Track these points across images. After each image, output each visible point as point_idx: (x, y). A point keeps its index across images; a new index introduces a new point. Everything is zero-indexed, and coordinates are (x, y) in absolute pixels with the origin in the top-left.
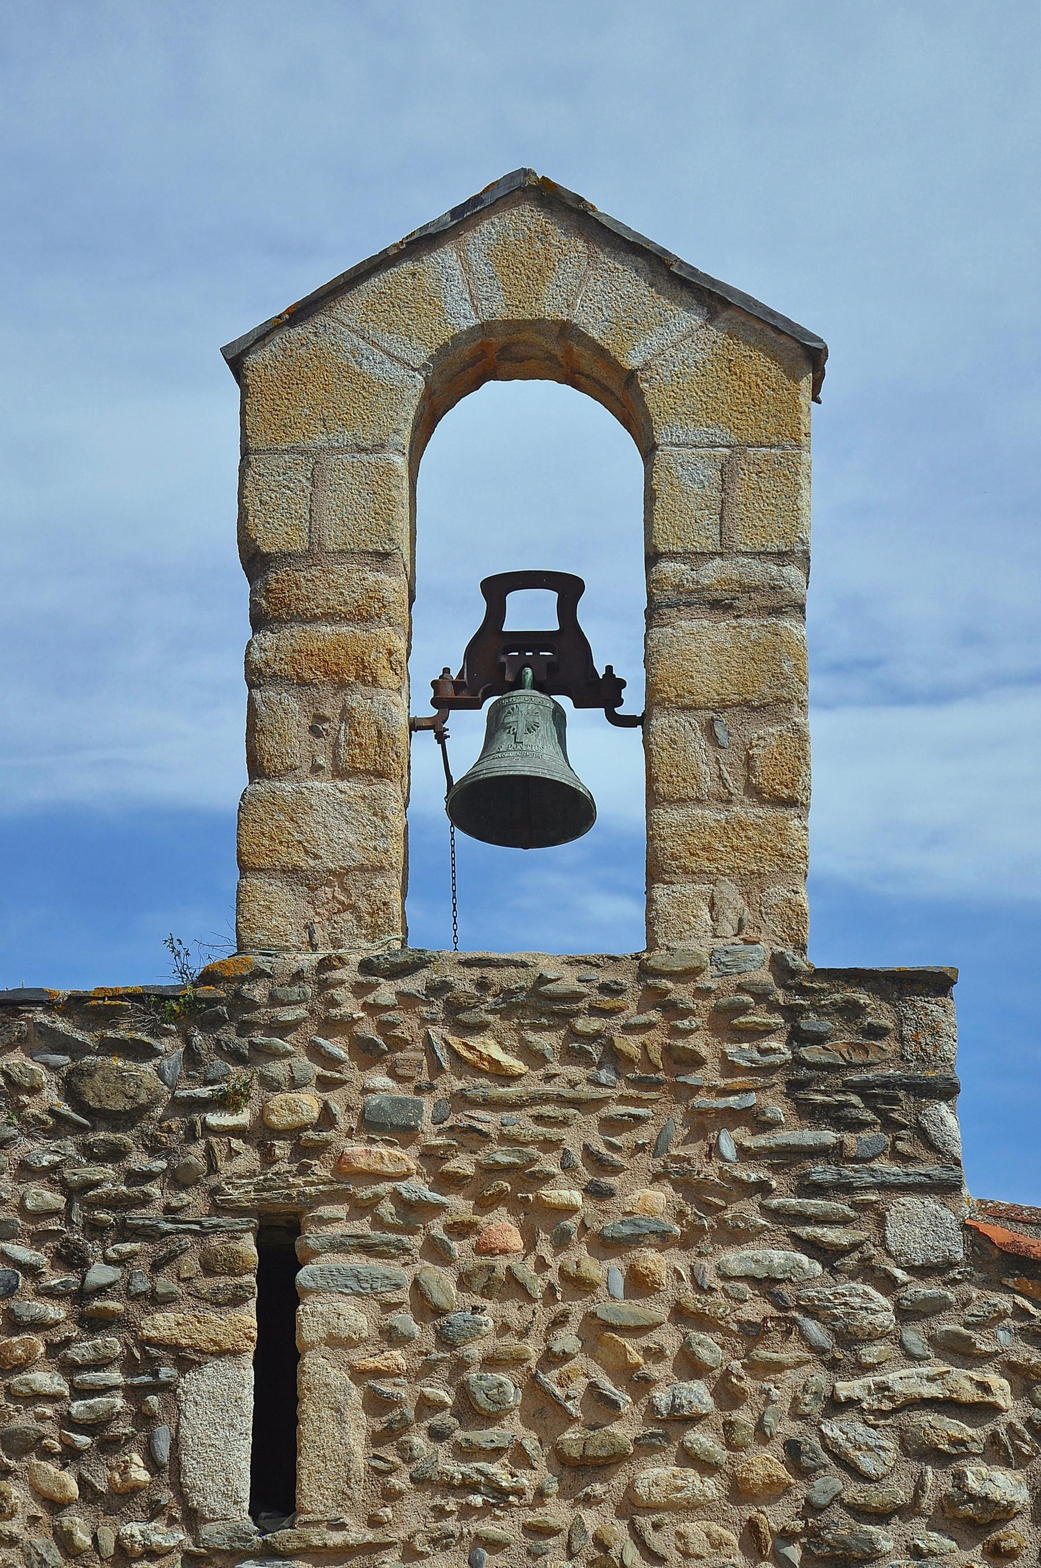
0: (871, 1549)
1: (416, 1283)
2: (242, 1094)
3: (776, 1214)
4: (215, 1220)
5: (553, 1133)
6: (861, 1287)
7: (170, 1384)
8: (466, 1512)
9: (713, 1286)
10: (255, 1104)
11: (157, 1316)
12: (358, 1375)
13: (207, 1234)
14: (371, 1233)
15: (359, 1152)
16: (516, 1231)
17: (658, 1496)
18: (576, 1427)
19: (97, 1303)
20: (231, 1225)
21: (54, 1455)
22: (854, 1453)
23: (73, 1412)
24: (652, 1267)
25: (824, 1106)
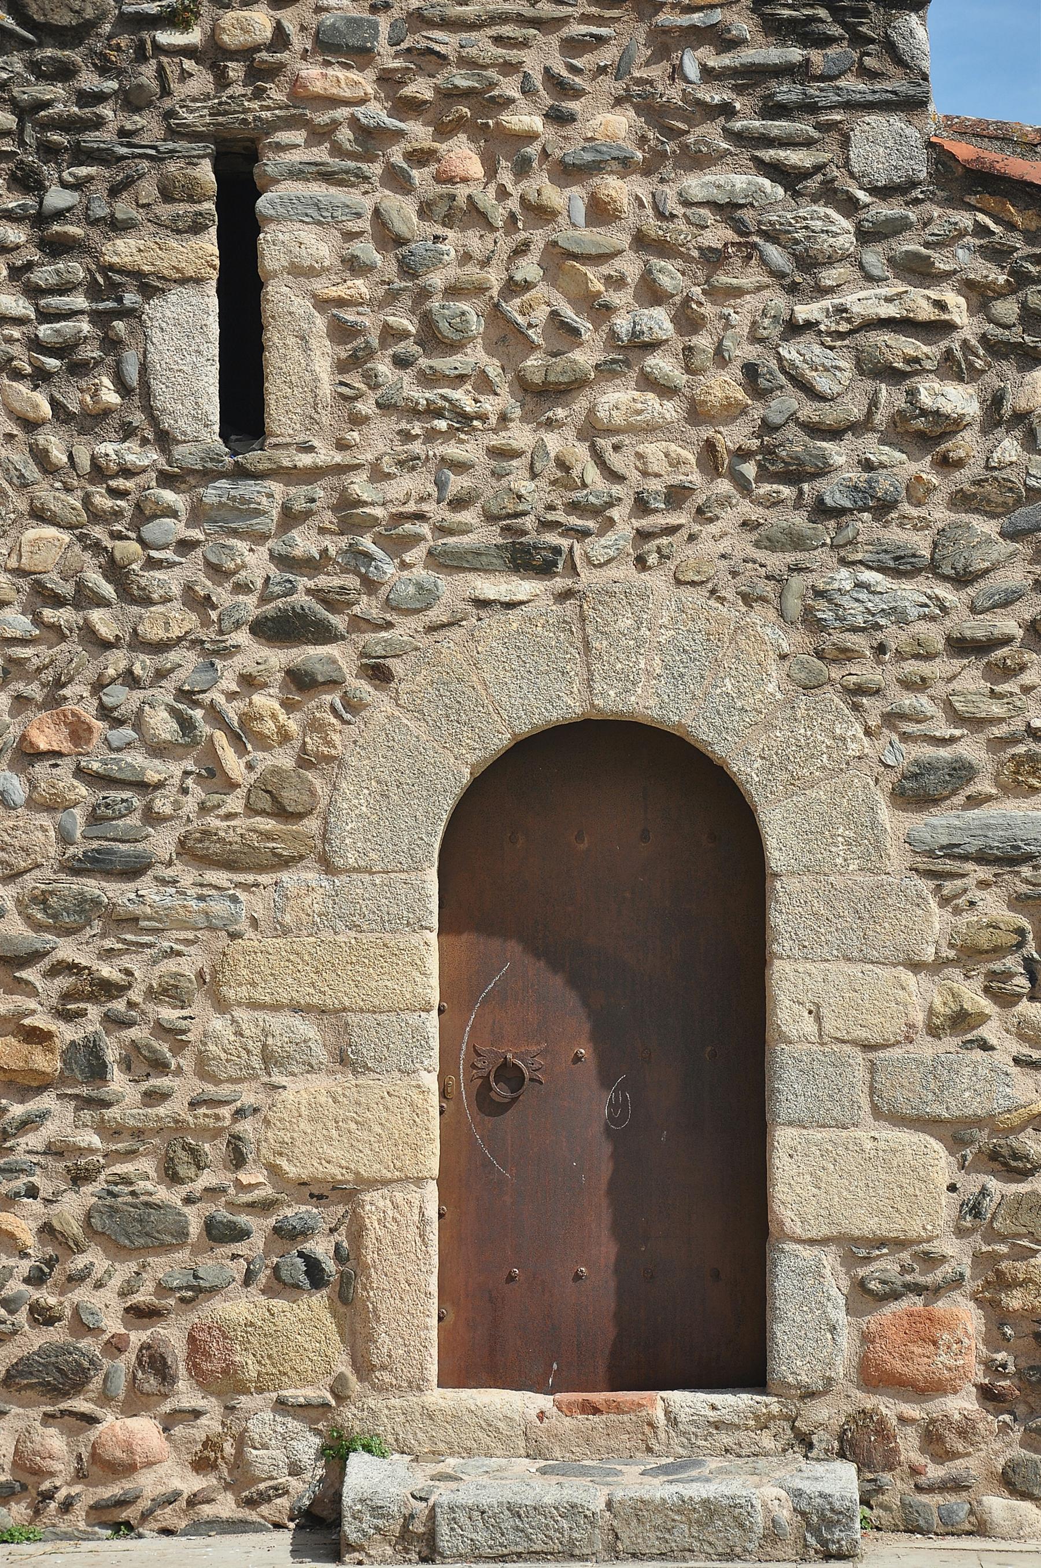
0: (824, 463)
1: (377, 212)
2: (191, 11)
3: (739, 138)
4: (171, 145)
5: (513, 55)
6: (822, 210)
7: (135, 310)
8: (432, 435)
9: (675, 212)
10: (206, 21)
11: (118, 242)
12: (322, 304)
13: (164, 159)
14: (330, 160)
15: (317, 77)
16: (476, 159)
17: (618, 418)
18: (538, 354)
19: (56, 228)
20: (188, 150)
21: (24, 376)
22: (810, 374)
23: (41, 335)
24: (614, 194)
25: (792, 20)
